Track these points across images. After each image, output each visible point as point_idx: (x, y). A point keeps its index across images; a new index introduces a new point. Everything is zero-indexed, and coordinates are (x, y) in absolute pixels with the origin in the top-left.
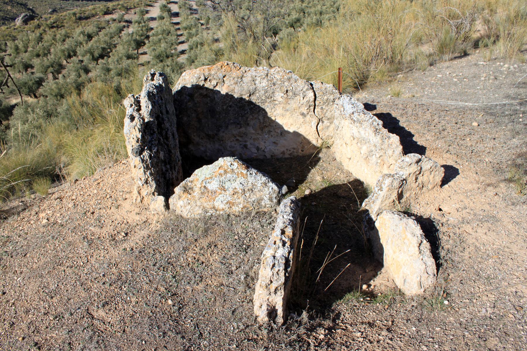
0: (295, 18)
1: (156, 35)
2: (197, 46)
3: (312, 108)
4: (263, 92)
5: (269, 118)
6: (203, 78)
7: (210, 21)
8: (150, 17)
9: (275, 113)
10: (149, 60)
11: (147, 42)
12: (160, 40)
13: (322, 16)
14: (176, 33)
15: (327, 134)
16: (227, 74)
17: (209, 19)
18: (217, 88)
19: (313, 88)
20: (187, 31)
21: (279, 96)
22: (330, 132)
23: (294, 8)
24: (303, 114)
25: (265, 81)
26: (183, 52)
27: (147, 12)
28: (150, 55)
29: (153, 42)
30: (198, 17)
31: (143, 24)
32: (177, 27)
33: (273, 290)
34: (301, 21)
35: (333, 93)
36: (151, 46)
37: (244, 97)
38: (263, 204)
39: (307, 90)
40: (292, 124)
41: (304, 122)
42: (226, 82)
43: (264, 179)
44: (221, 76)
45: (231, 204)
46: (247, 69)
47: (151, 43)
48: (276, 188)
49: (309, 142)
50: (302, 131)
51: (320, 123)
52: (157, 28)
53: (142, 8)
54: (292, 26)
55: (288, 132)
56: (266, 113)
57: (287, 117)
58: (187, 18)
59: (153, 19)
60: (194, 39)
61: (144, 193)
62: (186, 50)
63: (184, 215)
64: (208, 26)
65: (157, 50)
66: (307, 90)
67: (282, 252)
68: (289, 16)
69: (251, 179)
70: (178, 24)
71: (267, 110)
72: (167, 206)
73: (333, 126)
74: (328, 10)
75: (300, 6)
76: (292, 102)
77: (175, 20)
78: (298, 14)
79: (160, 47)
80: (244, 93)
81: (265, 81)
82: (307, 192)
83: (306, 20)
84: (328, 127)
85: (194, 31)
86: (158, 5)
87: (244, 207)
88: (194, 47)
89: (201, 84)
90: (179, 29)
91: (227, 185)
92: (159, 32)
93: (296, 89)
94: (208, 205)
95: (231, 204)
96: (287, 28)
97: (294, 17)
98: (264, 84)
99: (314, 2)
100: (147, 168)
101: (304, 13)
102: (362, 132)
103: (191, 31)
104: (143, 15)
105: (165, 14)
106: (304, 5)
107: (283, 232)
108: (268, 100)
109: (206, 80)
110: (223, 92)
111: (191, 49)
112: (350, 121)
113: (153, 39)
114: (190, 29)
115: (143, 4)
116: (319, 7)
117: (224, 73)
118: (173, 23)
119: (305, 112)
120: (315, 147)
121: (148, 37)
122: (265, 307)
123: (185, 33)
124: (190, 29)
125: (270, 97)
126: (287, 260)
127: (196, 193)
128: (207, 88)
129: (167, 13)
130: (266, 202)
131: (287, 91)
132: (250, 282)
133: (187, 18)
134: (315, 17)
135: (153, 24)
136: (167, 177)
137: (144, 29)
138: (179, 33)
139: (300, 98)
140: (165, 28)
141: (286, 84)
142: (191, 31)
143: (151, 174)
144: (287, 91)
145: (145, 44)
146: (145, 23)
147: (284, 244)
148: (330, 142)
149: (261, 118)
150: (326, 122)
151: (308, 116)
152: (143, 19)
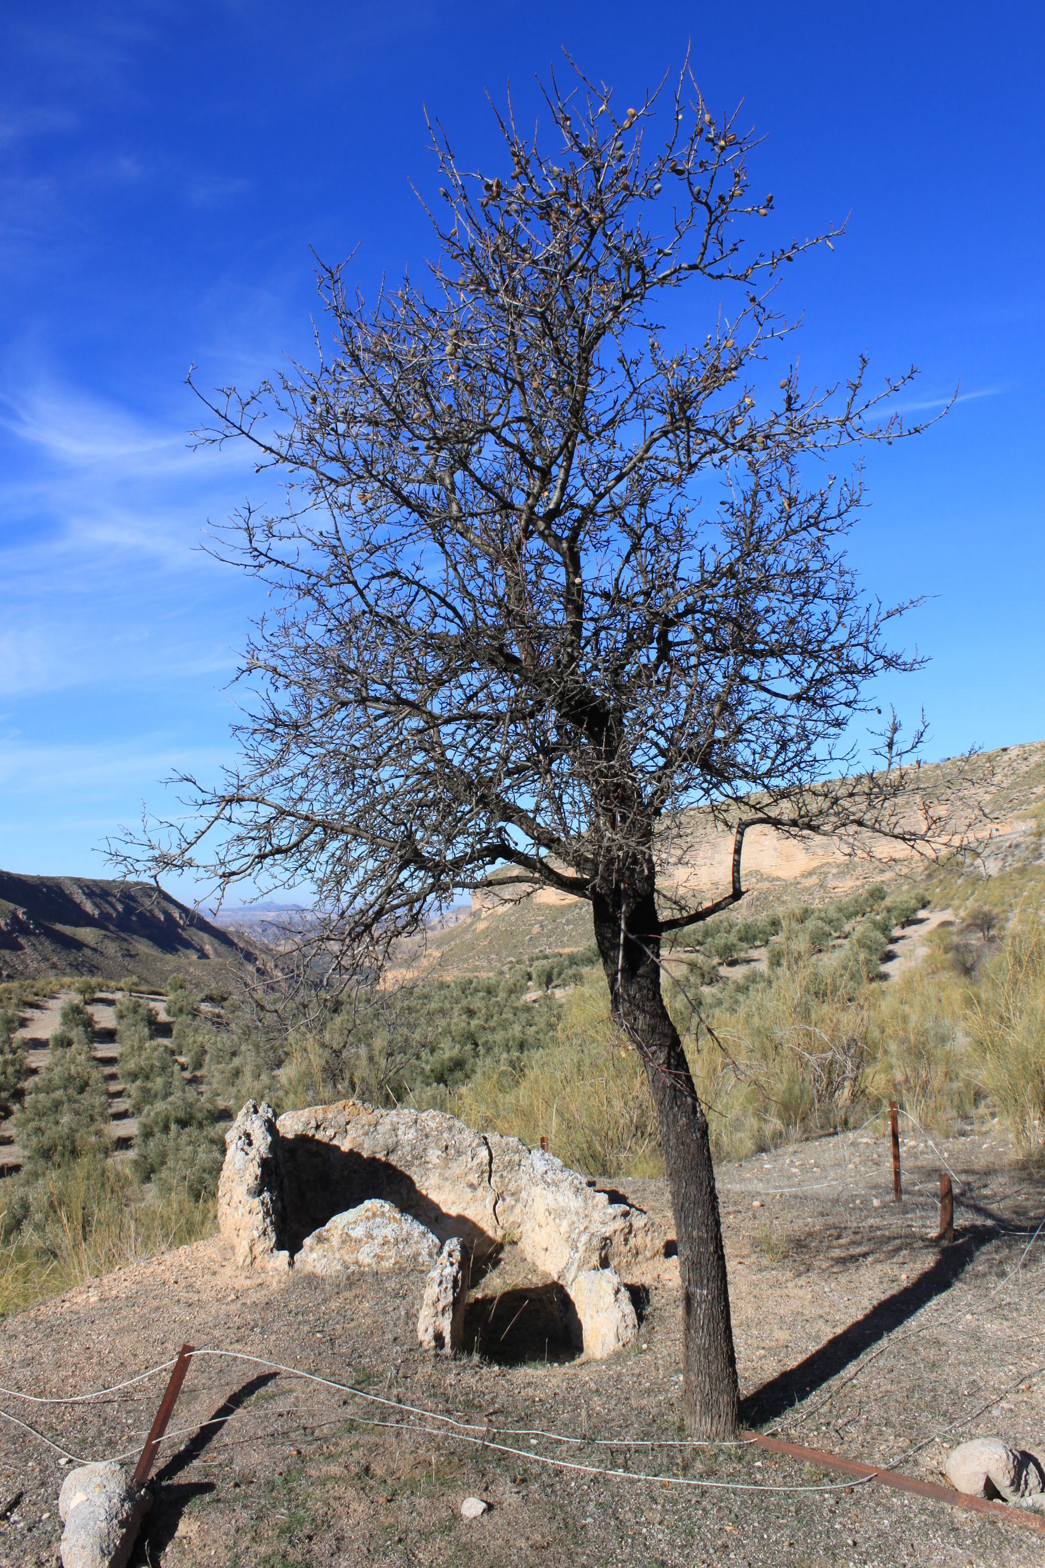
0: (451, 1059)
1: (48, 1089)
2: (166, 1129)
3: (486, 1175)
4: (409, 1148)
5: (418, 1193)
6: (313, 1124)
7: (207, 1058)
8: (29, 1036)
9: (427, 1184)
10: (20, 1161)
11: (16, 1107)
12: (57, 1105)
13: (526, 1053)
14: (104, 1086)
15: (511, 1219)
16: (354, 1119)
17: (205, 1052)
18: (335, 1142)
19: (487, 1144)
20: (138, 1083)
21: (434, 1155)
22: (516, 1216)
23: (447, 1032)
24: (472, 1186)
25: (412, 1130)
26: (124, 1143)
27: (23, 1023)
28: (25, 1147)
29: (35, 1107)
30: (170, 1045)
31: (10, 1056)
32: (108, 1070)
33: (440, 1308)
34: (468, 1067)
35: (518, 1151)
36: (29, 1121)
37: (378, 1156)
38: (420, 1260)
39: (478, 1145)
40: (454, 1203)
41: (474, 1199)
42: (350, 1132)
43: (422, 1228)
44: (342, 1120)
45: (379, 1258)
46: (384, 1112)
47: (29, 1113)
48: (437, 1241)
49: (481, 1232)
50: (470, 1214)
51: (500, 1202)
52: (49, 1069)
53: (10, 1012)
54: (441, 1079)
55: (448, 1216)
56: (413, 1183)
57: (447, 1189)
58: (141, 1048)
59: (37, 1044)
60: (160, 1106)
61: (258, 1249)
62: (130, 1139)
63: (318, 1271)
64: (198, 1073)
65: (48, 1133)
66: (478, 1145)
67: (450, 1271)
68: (432, 1051)
69: (406, 1227)
70: (110, 1061)
71: (415, 1178)
72: (291, 1264)
73: (520, 1206)
74: (541, 1036)
75: (463, 1025)
76: (454, 1165)
77: (104, 1050)
78: (458, 1046)
79: (57, 1123)
80: (378, 1149)
81: (412, 1130)
82: (480, 1296)
83: (480, 1063)
84: (513, 1207)
85: (159, 1082)
86: (57, 1006)
87: (396, 1263)
88: (156, 1130)
89: (310, 1133)
90: (113, 1077)
91: (375, 1233)
92: (57, 1081)
93: (461, 1143)
94: (349, 1258)
95: (379, 1258)
96: (428, 1084)
97: (447, 1055)
98: (410, 1136)
99: (504, 1016)
100: (267, 1214)
101: (476, 1045)
102: (560, 1199)
103: (149, 1085)
104: (13, 1030)
105: (77, 1033)
106: (474, 1022)
107: (450, 1255)
108: (417, 1162)
109: (318, 1127)
110: (345, 1147)
111: (147, 1134)
112: (542, 1185)
113: (37, 1101)
114: (147, 1078)
115: (14, 1001)
116: (517, 1028)
117: (348, 1118)
118: (95, 1059)
119: (475, 1182)
120: (491, 1241)
121: (19, 1095)
122: (431, 1330)
123: (133, 1088)
124: (147, 1078)
125: (420, 1157)
126: (455, 1281)
127: (335, 1241)
128: (318, 1142)
129: (81, 1028)
130: (424, 1257)
131: (447, 1147)
132: (411, 1317)
133: (141, 1048)
134: (505, 1055)
135: (37, 1059)
136: (289, 1232)
137: (10, 1070)
138: (114, 1087)
139: (466, 1158)
140: (73, 1071)
141: (445, 1135)
142: (149, 1085)
143: (272, 1222)
144: (447, 1147)
145: (8, 1113)
146: (14, 1052)
147: (452, 1264)
148: (517, 1233)
149: (404, 1191)
150: (508, 1199)
151: (480, 1189)
152: (9, 1041)
